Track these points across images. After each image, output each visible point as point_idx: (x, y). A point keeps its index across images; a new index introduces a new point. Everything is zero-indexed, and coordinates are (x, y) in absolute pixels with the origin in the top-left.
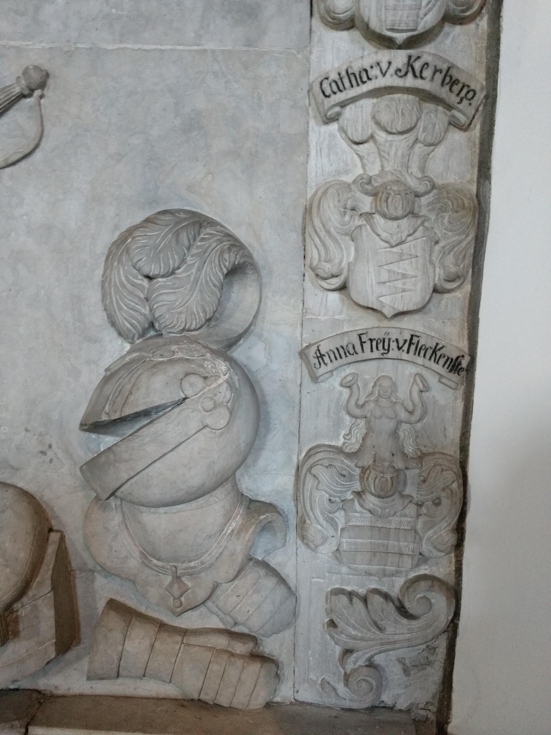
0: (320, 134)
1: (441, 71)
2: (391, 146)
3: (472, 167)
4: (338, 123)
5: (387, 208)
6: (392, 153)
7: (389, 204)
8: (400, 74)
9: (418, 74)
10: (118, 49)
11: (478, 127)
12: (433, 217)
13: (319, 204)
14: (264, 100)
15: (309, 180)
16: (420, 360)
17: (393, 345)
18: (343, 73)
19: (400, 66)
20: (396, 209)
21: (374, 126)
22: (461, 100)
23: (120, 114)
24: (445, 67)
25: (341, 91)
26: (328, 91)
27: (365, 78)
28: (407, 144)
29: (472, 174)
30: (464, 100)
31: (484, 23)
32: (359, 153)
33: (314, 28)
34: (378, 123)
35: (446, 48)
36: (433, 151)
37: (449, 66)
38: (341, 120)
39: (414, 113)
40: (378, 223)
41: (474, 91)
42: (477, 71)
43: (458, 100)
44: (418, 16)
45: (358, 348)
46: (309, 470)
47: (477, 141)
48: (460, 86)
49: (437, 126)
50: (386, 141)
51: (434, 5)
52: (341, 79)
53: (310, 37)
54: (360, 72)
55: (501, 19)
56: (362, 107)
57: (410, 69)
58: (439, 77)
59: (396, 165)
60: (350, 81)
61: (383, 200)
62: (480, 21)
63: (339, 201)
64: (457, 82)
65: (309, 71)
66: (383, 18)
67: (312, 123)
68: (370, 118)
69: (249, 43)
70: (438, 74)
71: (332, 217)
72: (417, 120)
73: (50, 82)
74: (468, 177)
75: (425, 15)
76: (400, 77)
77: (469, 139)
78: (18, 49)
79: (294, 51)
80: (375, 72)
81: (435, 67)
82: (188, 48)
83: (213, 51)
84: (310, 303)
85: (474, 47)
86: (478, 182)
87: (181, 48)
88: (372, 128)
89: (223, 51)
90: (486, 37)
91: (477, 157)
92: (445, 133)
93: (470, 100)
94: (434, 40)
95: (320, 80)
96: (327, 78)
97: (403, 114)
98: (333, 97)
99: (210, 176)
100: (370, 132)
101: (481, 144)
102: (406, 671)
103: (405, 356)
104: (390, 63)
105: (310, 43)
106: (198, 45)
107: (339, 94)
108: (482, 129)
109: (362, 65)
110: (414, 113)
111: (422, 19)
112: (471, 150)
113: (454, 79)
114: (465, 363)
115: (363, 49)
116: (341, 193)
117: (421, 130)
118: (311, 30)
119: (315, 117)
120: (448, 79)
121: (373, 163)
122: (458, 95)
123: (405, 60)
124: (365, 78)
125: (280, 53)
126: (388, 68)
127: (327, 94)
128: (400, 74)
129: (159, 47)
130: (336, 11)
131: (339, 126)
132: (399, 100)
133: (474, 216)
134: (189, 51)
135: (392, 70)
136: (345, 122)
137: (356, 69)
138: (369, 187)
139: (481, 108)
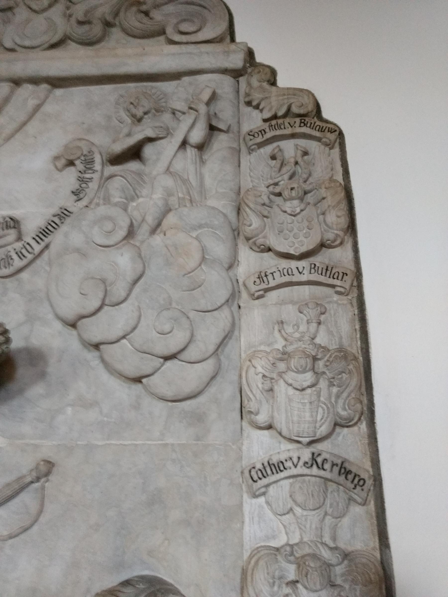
0: (250, 505)
1: (337, 465)
2: (306, 520)
3: (373, 534)
4: (265, 497)
5: (307, 582)
6: (308, 526)
7: (309, 580)
8: (307, 466)
9: (320, 466)
10: (106, 444)
11: (372, 502)
12: (347, 586)
13: (252, 574)
14: (208, 480)
15: (245, 544)
18: (266, 464)
19: (307, 460)
20: (315, 584)
21: (292, 502)
22: (355, 486)
23: (102, 493)
24: (339, 462)
25: (265, 477)
26: (255, 478)
27: (282, 468)
28: (319, 518)
29: (374, 542)
30: (358, 487)
31: (363, 426)
32: (283, 522)
33: (244, 428)
34: (294, 501)
35: (339, 443)
36: (340, 521)
37: (343, 460)
38: (266, 496)
39: (321, 494)
40: (302, 594)
41: (364, 480)
42: (364, 460)
43: (353, 486)
44: (315, 427)
47: (374, 514)
48: (353, 475)
49: (340, 504)
50: (302, 516)
51: (325, 421)
52: (264, 468)
53: (242, 433)
54: (278, 463)
55: (375, 424)
56: (282, 487)
57: (314, 462)
58: (336, 469)
59: (312, 536)
60: (271, 470)
61: (303, 575)
62: (360, 425)
63: (268, 574)
64: (350, 472)
65: (242, 457)
66: (291, 428)
67: (245, 496)
68: (288, 496)
69: (198, 439)
70: (335, 467)
71: (263, 588)
72: (324, 500)
73: (55, 470)
74: (372, 545)
75: (320, 427)
76: (308, 468)
77: (367, 512)
78: (36, 446)
79: (231, 444)
81: (333, 462)
82: (155, 443)
83: (173, 445)
85: (359, 443)
86: (381, 550)
87: (149, 442)
88: (290, 504)
89: (179, 445)
90: (366, 436)
91: (376, 528)
92: (347, 508)
93: (361, 486)
94: (330, 438)
95: (249, 468)
96: (254, 468)
97: (312, 495)
98: (259, 482)
99: (167, 542)
100: (289, 506)
101: (378, 517)
104: (299, 458)
105: (241, 437)
106: (162, 440)
107: (264, 479)
108: (376, 505)
109: (280, 459)
110: (321, 494)
111: (318, 429)
112: (369, 521)
113: (347, 470)
115: (280, 442)
116: (269, 566)
117: (328, 505)
118: (242, 429)
119: (247, 492)
120: (343, 471)
121: (294, 532)
122: (352, 482)
123: (310, 456)
124: (282, 468)
125: (221, 445)
126: (298, 462)
127: (255, 480)
128: (307, 466)
129: (135, 442)
130: (258, 423)
131: (266, 500)
132: (309, 481)
133: (380, 588)
134: (155, 445)
135: (301, 463)
136: (270, 498)
137: (275, 460)
138: (292, 558)
139: (372, 488)
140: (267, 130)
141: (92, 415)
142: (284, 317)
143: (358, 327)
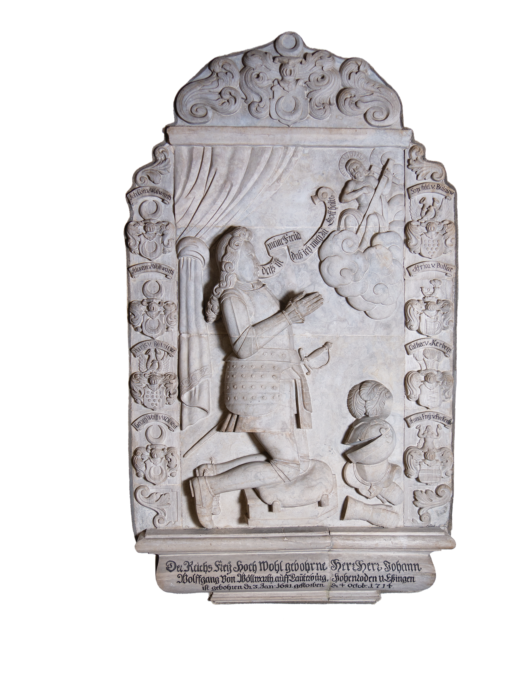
16: (439, 421)
17: (432, 417)
45: (422, 418)
46: (409, 453)
58: (441, 346)
78: (323, 336)
80: (424, 344)
84: (406, 405)
102: (438, 515)
103: (435, 420)
114: (452, 422)
140: (421, 189)
141: (345, 325)
142: (424, 285)
143: (454, 291)
